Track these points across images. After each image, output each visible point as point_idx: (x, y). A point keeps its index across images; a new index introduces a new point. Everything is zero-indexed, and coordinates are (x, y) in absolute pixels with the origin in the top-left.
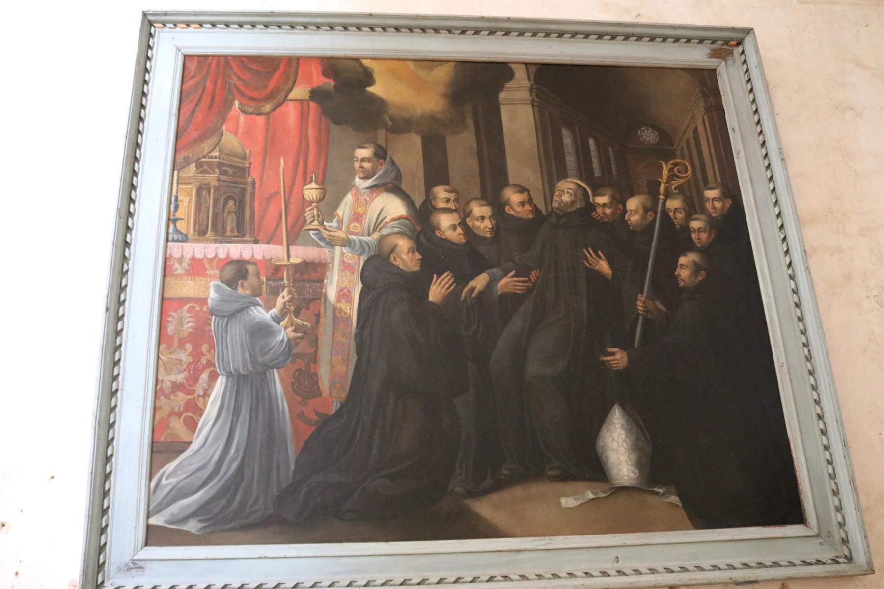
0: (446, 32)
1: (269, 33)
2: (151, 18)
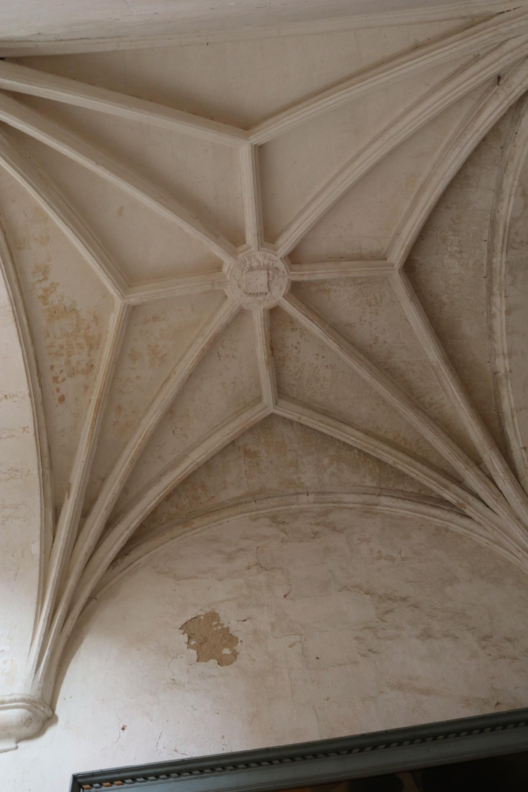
0: (334, 754)
1: (182, 780)
2: (80, 780)
